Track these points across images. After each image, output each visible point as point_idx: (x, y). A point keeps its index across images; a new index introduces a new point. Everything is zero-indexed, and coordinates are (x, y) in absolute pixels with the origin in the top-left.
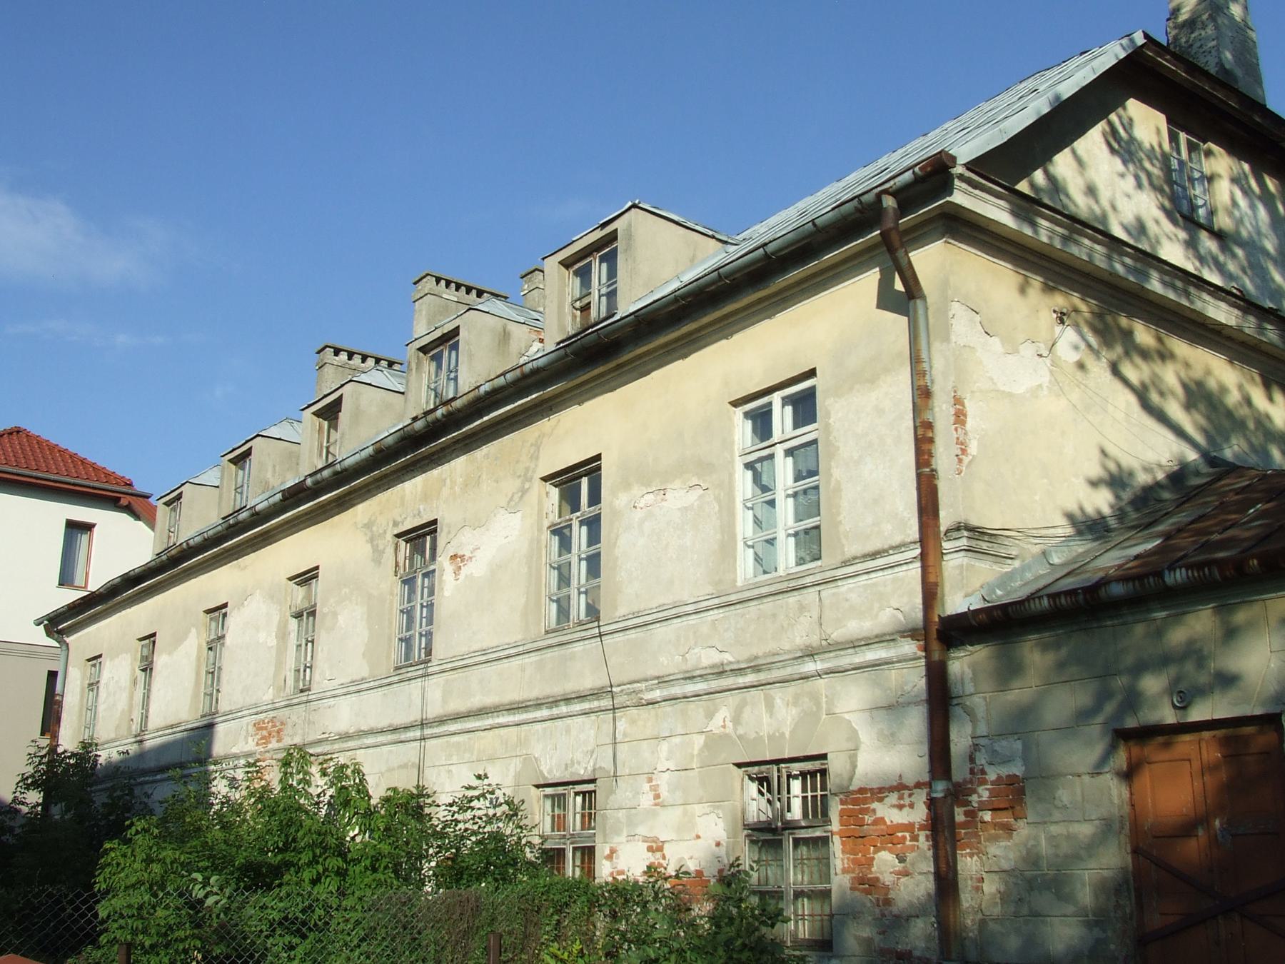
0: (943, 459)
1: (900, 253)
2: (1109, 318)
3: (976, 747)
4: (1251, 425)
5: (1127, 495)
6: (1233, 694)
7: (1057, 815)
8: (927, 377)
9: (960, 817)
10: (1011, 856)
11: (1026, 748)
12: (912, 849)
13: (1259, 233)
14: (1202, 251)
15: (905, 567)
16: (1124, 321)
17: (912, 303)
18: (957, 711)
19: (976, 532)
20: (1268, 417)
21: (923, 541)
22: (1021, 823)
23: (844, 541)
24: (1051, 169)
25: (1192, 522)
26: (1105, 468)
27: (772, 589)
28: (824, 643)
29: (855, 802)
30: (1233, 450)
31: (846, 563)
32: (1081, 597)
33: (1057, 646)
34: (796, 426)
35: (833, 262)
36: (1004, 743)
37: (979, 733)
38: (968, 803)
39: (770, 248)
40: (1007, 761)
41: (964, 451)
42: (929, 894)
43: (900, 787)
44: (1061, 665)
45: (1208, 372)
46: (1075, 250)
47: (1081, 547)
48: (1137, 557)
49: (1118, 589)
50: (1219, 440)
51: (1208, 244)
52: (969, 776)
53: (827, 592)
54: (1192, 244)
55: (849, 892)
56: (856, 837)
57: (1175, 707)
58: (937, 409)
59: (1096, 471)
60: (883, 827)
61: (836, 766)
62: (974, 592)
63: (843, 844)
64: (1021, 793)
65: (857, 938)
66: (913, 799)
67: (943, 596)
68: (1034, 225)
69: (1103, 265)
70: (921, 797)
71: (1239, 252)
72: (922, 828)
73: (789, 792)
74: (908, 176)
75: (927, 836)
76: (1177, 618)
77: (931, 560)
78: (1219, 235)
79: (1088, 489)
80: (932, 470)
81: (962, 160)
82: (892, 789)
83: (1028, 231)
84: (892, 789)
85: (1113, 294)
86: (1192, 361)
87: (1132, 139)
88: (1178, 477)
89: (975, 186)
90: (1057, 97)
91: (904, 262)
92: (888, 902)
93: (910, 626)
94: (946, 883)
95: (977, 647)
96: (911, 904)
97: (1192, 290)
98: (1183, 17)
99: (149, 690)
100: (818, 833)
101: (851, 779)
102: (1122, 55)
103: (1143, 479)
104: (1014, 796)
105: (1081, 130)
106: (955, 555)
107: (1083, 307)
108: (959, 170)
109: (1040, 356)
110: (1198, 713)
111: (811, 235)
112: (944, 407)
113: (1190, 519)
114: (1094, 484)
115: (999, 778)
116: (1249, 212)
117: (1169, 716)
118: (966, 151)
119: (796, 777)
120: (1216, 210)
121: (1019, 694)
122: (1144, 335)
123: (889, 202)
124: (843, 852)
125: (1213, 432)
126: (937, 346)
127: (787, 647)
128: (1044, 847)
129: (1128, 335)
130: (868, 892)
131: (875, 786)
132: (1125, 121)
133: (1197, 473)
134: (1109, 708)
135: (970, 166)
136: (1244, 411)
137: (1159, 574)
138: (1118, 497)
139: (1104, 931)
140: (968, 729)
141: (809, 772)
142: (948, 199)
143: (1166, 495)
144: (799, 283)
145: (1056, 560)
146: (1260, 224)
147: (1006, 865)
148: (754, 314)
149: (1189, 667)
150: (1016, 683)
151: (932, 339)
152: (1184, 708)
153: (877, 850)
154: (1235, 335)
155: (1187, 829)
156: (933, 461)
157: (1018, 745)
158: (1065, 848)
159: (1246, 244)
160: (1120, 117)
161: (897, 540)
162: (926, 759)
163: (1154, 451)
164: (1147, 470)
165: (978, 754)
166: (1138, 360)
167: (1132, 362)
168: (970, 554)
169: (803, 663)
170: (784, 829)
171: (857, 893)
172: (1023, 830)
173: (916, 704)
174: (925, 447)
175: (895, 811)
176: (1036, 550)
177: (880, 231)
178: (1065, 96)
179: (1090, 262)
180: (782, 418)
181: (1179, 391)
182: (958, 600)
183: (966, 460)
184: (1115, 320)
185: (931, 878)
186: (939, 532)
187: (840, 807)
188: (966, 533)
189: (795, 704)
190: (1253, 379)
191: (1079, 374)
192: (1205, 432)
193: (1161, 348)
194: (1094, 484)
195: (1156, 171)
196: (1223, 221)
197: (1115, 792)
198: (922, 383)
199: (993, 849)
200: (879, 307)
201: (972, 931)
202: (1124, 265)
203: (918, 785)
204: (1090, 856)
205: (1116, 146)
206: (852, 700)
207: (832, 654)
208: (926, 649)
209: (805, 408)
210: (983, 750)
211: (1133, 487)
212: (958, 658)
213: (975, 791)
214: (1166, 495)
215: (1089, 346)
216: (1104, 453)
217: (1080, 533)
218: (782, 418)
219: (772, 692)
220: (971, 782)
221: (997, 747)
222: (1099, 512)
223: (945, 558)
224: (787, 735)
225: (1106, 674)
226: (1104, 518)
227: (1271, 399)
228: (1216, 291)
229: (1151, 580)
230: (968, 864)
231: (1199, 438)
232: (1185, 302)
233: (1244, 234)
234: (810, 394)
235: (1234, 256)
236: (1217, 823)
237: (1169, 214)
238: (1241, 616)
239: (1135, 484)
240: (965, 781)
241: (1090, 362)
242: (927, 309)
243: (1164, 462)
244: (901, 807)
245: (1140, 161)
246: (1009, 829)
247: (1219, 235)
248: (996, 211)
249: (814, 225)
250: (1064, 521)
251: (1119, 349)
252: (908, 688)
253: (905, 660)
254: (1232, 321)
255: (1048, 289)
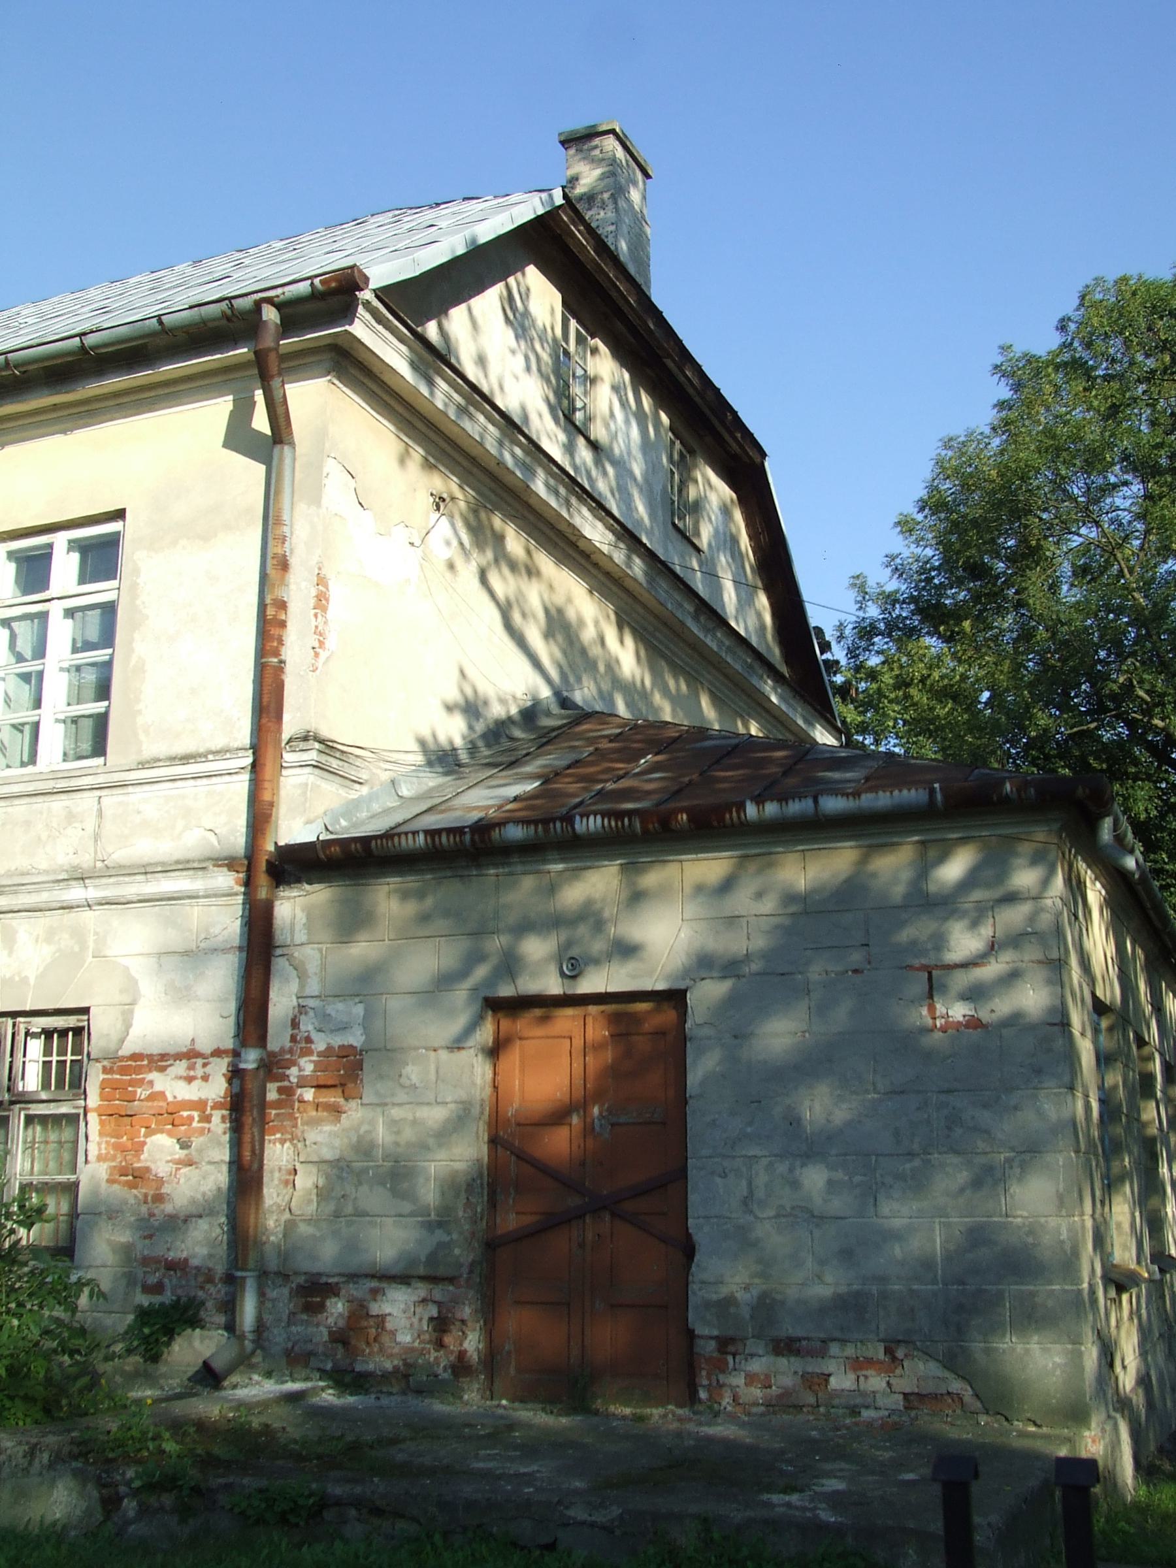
0: (295, 649)
1: (276, 383)
2: (483, 515)
3: (302, 1009)
4: (602, 668)
5: (480, 727)
6: (631, 966)
7: (402, 1097)
8: (287, 544)
9: (272, 1095)
10: (337, 1143)
11: (368, 1015)
12: (201, 1132)
13: (629, 453)
14: (578, 461)
15: (227, 778)
16: (497, 522)
17: (277, 448)
18: (280, 964)
19: (328, 746)
20: (618, 661)
21: (256, 748)
22: (353, 1104)
23: (142, 737)
24: (445, 323)
25: (569, 767)
26: (462, 691)
27: (30, 788)
28: (99, 864)
29: (124, 1071)
30: (584, 694)
31: (143, 765)
32: (468, 837)
33: (421, 895)
34: (82, 580)
35: (168, 377)
36: (340, 1006)
37: (308, 992)
38: (285, 1077)
39: (90, 340)
40: (343, 1028)
41: (321, 643)
42: (219, 1189)
43: (191, 1055)
44: (424, 918)
45: (569, 600)
46: (467, 425)
47: (432, 780)
48: (516, 799)
49: (515, 833)
50: (572, 679)
51: (585, 454)
52: (288, 1045)
53: (111, 800)
54: (570, 449)
55: (104, 1185)
56: (121, 1116)
57: (562, 974)
58: (292, 587)
59: (453, 695)
60: (164, 1104)
61: (102, 1026)
62: (317, 818)
63: (102, 1123)
64: (359, 1066)
65: (109, 1242)
66: (208, 1069)
67: (277, 818)
68: (431, 383)
69: (493, 451)
70: (220, 1067)
71: (610, 470)
72: (217, 1106)
73: (24, 1056)
74: (303, 288)
75: (223, 1117)
76: (575, 874)
77: (268, 772)
78: (594, 446)
79: (442, 712)
80: (281, 662)
81: (373, 285)
82: (179, 1057)
83: (424, 390)
84: (179, 1057)
85: (496, 487)
86: (556, 584)
87: (526, 313)
88: (530, 714)
89: (379, 319)
90: (474, 240)
91: (278, 395)
92: (159, 1198)
93: (225, 854)
94: (246, 1178)
95: (317, 887)
96: (193, 1201)
97: (574, 500)
98: (579, 190)
99: (726, 676)
100: (64, 1109)
101: (122, 1041)
102: (541, 211)
103: (497, 711)
104: (347, 1071)
105: (480, 287)
106: (298, 770)
107: (458, 494)
108: (366, 295)
109: (412, 544)
110: (593, 983)
111: (153, 334)
112: (303, 585)
113: (565, 763)
114: (449, 708)
115: (329, 1048)
116: (623, 427)
117: (553, 986)
118: (383, 272)
119: (36, 1036)
120: (595, 417)
121: (363, 949)
122: (515, 543)
123: (270, 314)
124: (101, 1134)
125: (566, 669)
126: (301, 508)
127: (44, 865)
128: (381, 1134)
129: (500, 539)
130: (132, 1186)
131: (155, 1051)
132: (523, 290)
133: (548, 713)
134: (481, 972)
135: (380, 294)
136: (595, 651)
137: (568, 819)
138: (471, 727)
139: (449, 1234)
140: (294, 986)
141: (55, 1030)
142: (347, 327)
143: (518, 733)
144: (116, 395)
145: (405, 792)
146: (632, 444)
147: (328, 1154)
148: (23, 428)
149: (582, 930)
150: (363, 935)
151: (296, 498)
152: (574, 977)
153: (150, 1132)
154: (603, 563)
155: (558, 1116)
156: (283, 650)
157: (359, 1010)
158: (408, 1134)
159: (617, 463)
160: (518, 284)
161: (218, 743)
162: (232, 1021)
163: (513, 681)
164: (502, 701)
165: (303, 1017)
166: (506, 570)
167: (500, 571)
168: (317, 771)
169: (68, 888)
170: (12, 1103)
171: (116, 1187)
172: (354, 1113)
173: (225, 951)
174: (274, 631)
175: (182, 1084)
176: (385, 776)
177: (248, 348)
178: (483, 240)
179: (481, 444)
180: (65, 567)
181: (541, 615)
182: (295, 828)
183: (323, 655)
184: (489, 519)
185: (225, 1168)
186: (280, 740)
187: (102, 1077)
188: (317, 745)
189: (49, 939)
190: (608, 617)
191: (448, 575)
192: (560, 667)
193: (529, 562)
194: (449, 708)
195: (545, 357)
196: (598, 432)
197: (478, 1070)
198: (279, 551)
199: (312, 1135)
200: (227, 444)
201: (275, 1234)
202: (513, 455)
203: (217, 1053)
204: (440, 1146)
205: (511, 316)
206: (133, 940)
207: (112, 880)
208: (248, 883)
209: (101, 557)
210: (311, 1013)
211: (486, 719)
212: (289, 898)
213: (294, 1063)
214: (518, 733)
215: (461, 544)
216: (463, 674)
217: (430, 763)
218: (65, 567)
219: (14, 923)
220: (291, 1051)
221: (330, 1010)
222: (451, 743)
223: (284, 772)
224: (32, 981)
225: (479, 933)
226: (454, 749)
227: (622, 642)
228: (600, 508)
229: (558, 825)
230: (277, 1154)
231: (554, 674)
232: (565, 514)
233: (617, 451)
234: (112, 543)
235: (605, 473)
236: (596, 1110)
237: (552, 409)
238: (651, 879)
239: (489, 716)
240: (282, 1051)
241: (459, 563)
242: (294, 459)
243: (519, 695)
244: (190, 1080)
245: (532, 340)
246: (337, 1111)
247: (594, 446)
248: (393, 354)
249: (160, 322)
250: (415, 747)
251: (490, 555)
252: (216, 930)
253: (215, 896)
254: (605, 549)
255: (428, 466)
